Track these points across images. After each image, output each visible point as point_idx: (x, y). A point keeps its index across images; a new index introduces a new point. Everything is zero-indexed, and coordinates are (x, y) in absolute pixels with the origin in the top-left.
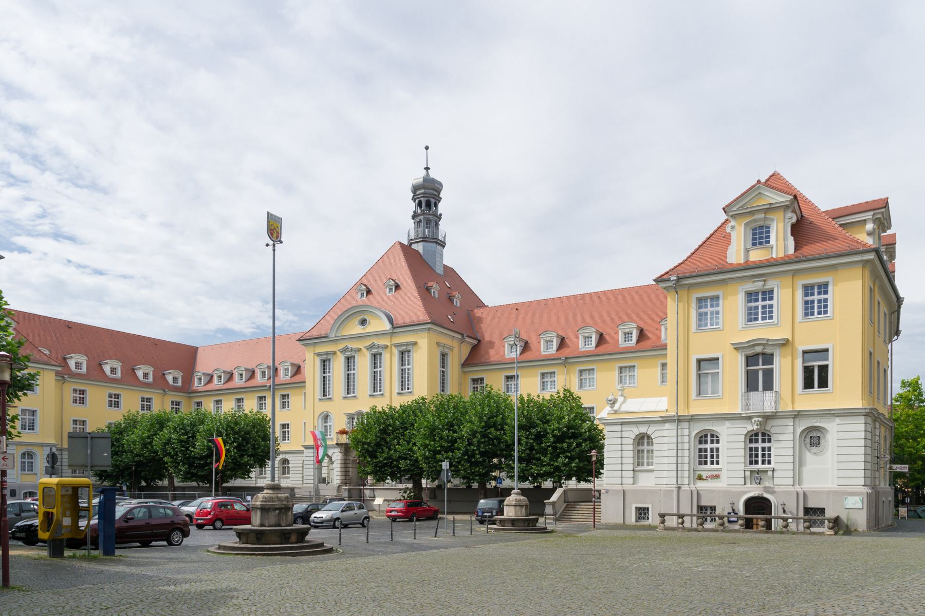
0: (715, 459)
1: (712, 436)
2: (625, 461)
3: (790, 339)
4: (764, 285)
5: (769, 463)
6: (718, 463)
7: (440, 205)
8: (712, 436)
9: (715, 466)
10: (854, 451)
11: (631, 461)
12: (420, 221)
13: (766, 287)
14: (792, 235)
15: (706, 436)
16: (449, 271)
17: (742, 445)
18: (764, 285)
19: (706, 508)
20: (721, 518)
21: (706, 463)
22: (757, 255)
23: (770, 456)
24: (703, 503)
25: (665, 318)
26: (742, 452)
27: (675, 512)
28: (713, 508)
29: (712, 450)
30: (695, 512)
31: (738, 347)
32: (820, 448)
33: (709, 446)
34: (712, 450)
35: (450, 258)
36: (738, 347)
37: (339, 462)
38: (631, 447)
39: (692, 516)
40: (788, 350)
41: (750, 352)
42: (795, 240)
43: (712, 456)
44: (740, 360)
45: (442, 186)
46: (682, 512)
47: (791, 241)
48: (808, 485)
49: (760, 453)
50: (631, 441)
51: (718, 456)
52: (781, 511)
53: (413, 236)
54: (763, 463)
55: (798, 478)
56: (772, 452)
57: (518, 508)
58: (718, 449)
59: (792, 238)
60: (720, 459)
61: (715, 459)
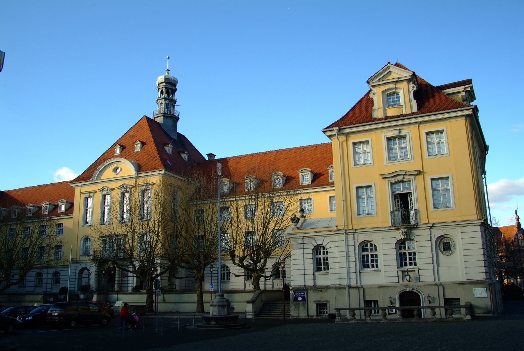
0: (375, 263)
1: (371, 245)
2: (306, 267)
3: (421, 170)
4: (400, 133)
5: (415, 264)
6: (377, 266)
7: (176, 94)
8: (371, 245)
9: (375, 269)
10: (29, 285)
11: (311, 266)
12: (162, 103)
13: (400, 134)
14: (415, 98)
15: (367, 245)
16: (182, 138)
17: (394, 251)
18: (400, 133)
19: (370, 302)
20: (384, 309)
21: (368, 267)
22: (391, 112)
23: (415, 259)
24: (368, 298)
25: (331, 162)
26: (395, 257)
27: (347, 307)
28: (376, 302)
29: (372, 256)
30: (362, 306)
31: (385, 177)
32: (450, 252)
33: (369, 253)
34: (372, 256)
35: (181, 129)
36: (385, 177)
37: (94, 273)
38: (311, 256)
39: (360, 309)
40: (421, 177)
41: (393, 180)
42: (417, 102)
43: (372, 261)
44: (386, 184)
45: (177, 82)
46: (352, 306)
47: (414, 102)
48: (445, 277)
49: (370, 259)
50: (311, 251)
51: (377, 261)
52: (427, 302)
53: (156, 113)
54: (411, 264)
55: (436, 272)
56: (329, 261)
57: (220, 307)
58: (376, 255)
59: (415, 101)
60: (379, 263)
61: (375, 263)
